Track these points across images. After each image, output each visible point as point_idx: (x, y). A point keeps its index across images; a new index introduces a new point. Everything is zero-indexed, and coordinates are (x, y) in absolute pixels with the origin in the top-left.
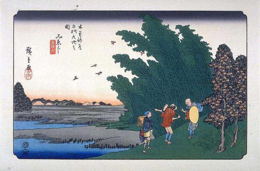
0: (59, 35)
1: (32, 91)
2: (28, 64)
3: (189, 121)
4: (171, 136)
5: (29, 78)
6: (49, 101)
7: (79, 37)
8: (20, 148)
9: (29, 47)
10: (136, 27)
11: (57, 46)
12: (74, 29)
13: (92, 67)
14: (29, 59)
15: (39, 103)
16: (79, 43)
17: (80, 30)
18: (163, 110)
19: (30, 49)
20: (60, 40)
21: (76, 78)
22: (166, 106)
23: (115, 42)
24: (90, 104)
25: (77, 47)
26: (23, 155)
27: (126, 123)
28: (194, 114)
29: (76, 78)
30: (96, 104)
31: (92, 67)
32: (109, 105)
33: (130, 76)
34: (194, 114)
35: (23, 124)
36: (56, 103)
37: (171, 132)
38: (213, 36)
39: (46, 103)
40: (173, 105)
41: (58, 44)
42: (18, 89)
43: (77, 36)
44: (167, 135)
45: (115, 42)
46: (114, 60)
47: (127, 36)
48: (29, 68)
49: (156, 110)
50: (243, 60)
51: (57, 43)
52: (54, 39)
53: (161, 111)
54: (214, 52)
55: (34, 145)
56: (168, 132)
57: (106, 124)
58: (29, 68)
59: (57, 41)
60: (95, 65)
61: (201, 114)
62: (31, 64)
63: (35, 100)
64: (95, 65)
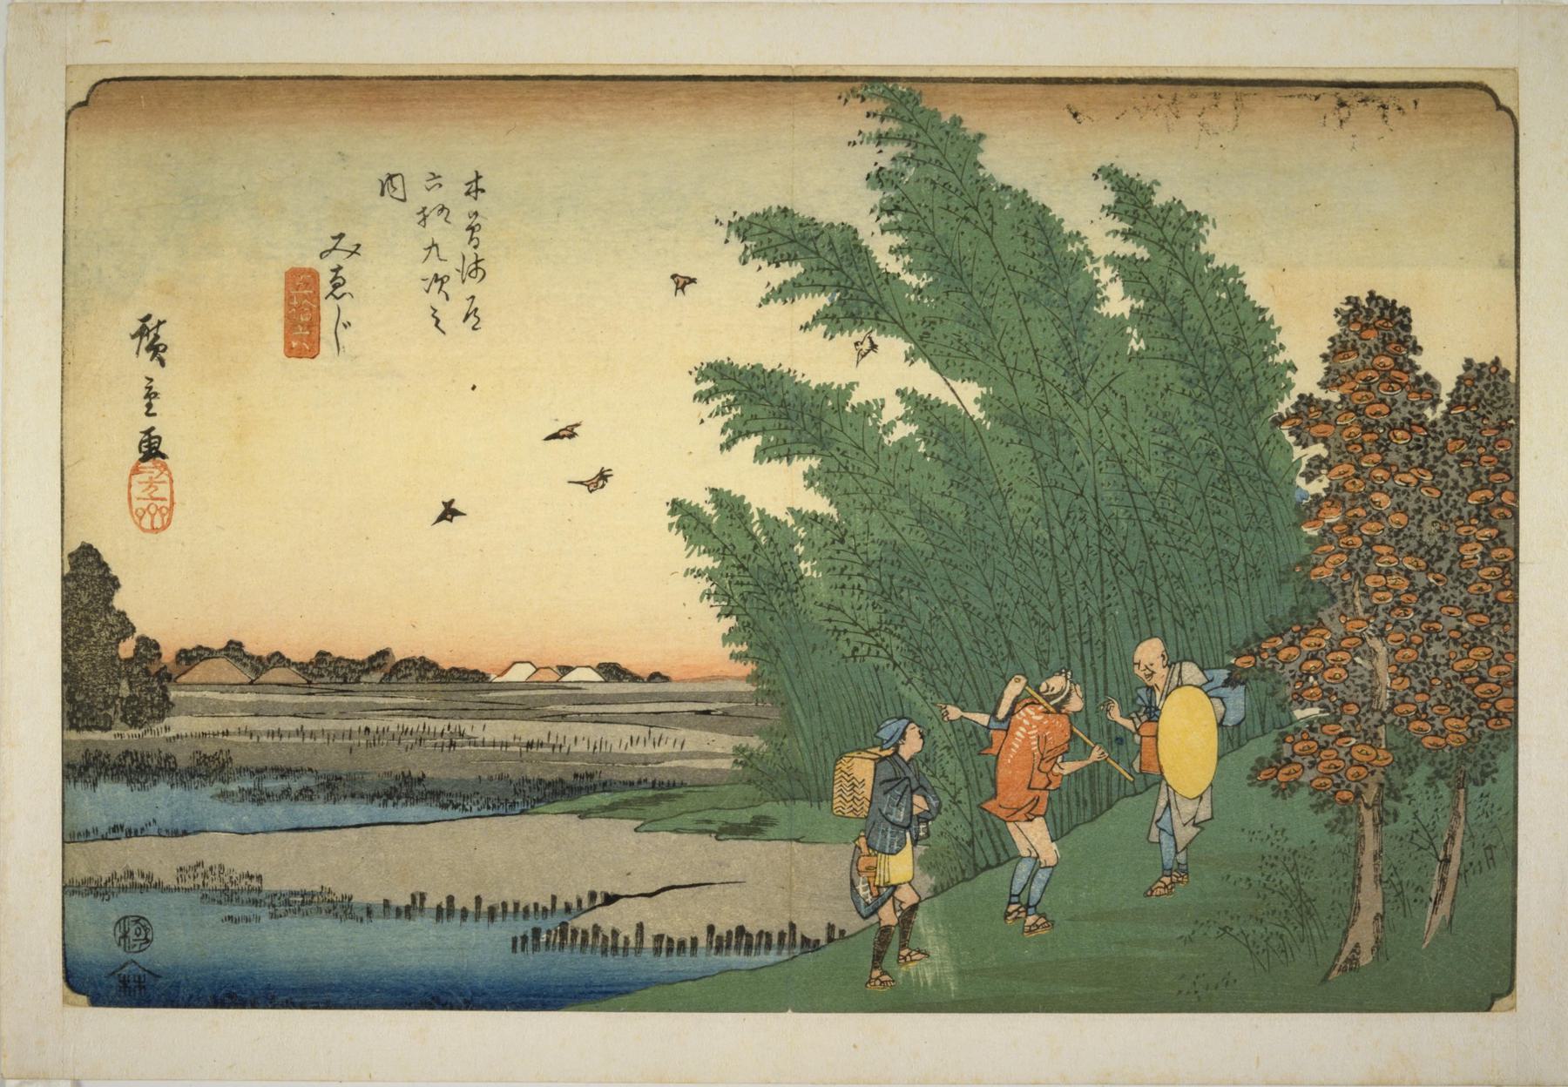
0: (341, 236)
1: (162, 603)
2: (148, 423)
3: (1153, 780)
4: (1042, 875)
5: (158, 524)
6: (278, 659)
7: (470, 252)
8: (101, 947)
9: (148, 317)
10: (834, 179)
11: (328, 309)
12: (433, 199)
13: (555, 436)
14: (151, 395)
15: (224, 670)
16: (472, 286)
17: (470, 205)
18: (994, 714)
19: (157, 327)
20: (350, 268)
21: (449, 512)
22: (1014, 689)
23: (693, 281)
24: (541, 676)
25: (451, 314)
26: (114, 978)
27: (769, 794)
28: (1188, 735)
29: (449, 512)
30: (571, 677)
31: (555, 436)
32: (655, 677)
33: (780, 489)
34: (1188, 735)
35: (115, 799)
36: (328, 671)
37: (1049, 852)
38: (1296, 260)
39: (257, 672)
40: (1057, 683)
41: (338, 292)
42: (88, 579)
43: (454, 243)
44: (1024, 869)
45: (693, 281)
46: (737, 247)
47: (772, 235)
48: (151, 450)
49: (954, 712)
50: (1491, 393)
51: (325, 287)
52: (307, 265)
53: (983, 719)
54: (1304, 350)
55: (184, 937)
56: (1024, 853)
57: (650, 796)
58: (151, 450)
59: (325, 278)
60: (569, 433)
61: (1231, 737)
62: (161, 427)
63: (191, 657)
64: (569, 433)
